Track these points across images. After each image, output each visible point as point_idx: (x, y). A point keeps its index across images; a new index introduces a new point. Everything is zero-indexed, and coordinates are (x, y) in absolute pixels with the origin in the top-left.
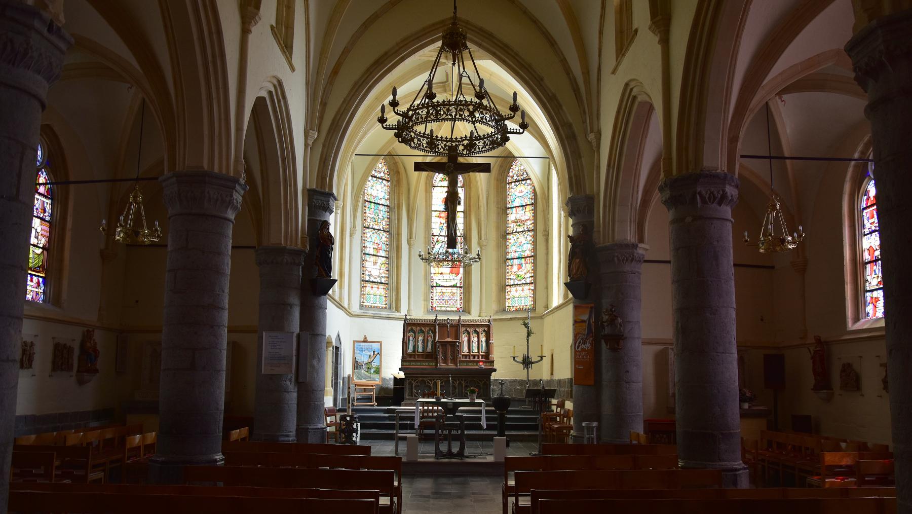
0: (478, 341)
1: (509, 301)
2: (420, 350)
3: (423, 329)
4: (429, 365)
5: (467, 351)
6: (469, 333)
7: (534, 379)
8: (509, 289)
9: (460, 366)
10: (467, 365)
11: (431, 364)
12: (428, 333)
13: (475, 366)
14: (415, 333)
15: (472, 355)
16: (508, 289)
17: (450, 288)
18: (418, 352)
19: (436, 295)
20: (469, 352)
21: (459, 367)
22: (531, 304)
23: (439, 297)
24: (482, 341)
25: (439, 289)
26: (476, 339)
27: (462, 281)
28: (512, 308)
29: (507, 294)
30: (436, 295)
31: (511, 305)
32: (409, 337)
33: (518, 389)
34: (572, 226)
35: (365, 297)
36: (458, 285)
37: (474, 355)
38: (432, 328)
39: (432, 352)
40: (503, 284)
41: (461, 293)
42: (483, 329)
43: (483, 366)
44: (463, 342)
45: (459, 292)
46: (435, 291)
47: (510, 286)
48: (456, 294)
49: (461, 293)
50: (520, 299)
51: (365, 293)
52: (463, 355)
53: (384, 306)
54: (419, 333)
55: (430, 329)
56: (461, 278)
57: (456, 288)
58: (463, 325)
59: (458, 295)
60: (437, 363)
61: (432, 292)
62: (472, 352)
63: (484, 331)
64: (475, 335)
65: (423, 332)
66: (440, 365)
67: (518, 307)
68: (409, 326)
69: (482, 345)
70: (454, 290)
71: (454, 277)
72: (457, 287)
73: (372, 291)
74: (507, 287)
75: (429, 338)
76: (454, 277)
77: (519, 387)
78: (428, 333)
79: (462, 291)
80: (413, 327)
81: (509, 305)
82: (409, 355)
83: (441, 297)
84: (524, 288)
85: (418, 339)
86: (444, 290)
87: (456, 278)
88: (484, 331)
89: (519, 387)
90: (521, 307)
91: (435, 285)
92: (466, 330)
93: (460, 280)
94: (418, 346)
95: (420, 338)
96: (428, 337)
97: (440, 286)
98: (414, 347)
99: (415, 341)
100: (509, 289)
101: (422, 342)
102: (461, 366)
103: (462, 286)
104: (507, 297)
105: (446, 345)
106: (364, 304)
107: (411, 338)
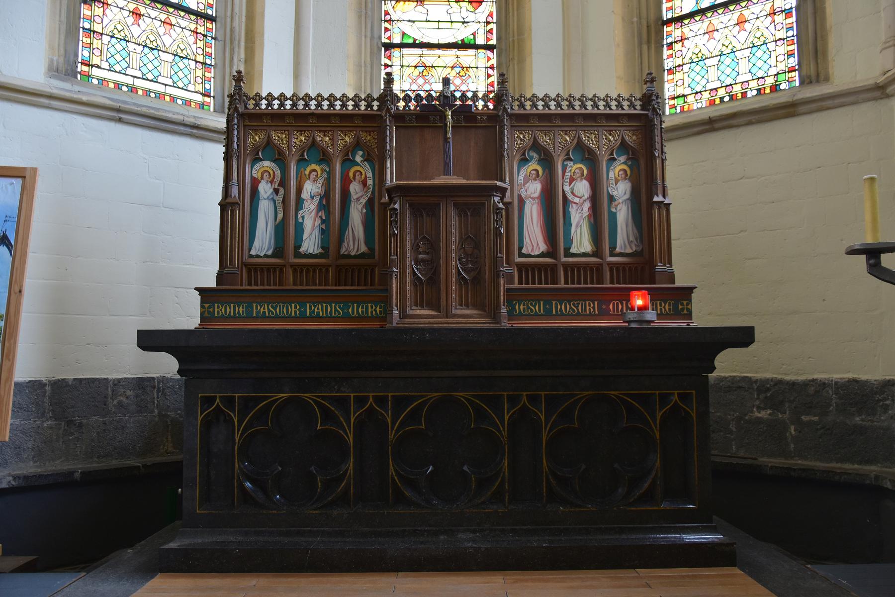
0: (595, 199)
1: (678, 76)
2: (310, 243)
3: (323, 139)
4: (347, 318)
5: (543, 247)
6: (547, 160)
7: (850, 376)
8: (677, 33)
9: (511, 315)
10: (548, 314)
11: (355, 310)
12: (348, 161)
13: (591, 316)
14: (280, 159)
15: (566, 266)
16: (673, 32)
17: (453, 51)
18: (298, 255)
19: (402, 77)
20: (552, 252)
21: (506, 324)
22: (782, 67)
23: (414, 81)
24: (611, 198)
25: (411, 56)
26: (583, 188)
27: (493, 26)
28: (691, 99)
29: (666, 53)
30: (402, 77)
31: (688, 91)
32: (255, 183)
33: (759, 421)
34: (606, 161)
35: (97, 43)
36: (481, 41)
37: (578, 266)
38: (366, 137)
39: (370, 254)
40: (652, 17)
41: (492, 68)
42: (613, 139)
43: (651, 315)
44: (522, 202)
45: (482, 63)
46: (396, 61)
47: (680, 19)
48: (472, 72)
49: (492, 68)
50: (728, 61)
51: (97, 28)
52: (521, 267)
53: (198, 98)
54: (301, 161)
55: (358, 145)
56: (491, 15)
57: (472, 52)
58: (522, 120)
59: (482, 73)
60: (386, 301)
61: (386, 66)
62: (568, 253)
63: (624, 147)
64: (576, 167)
65: (325, 158)
66: (404, 315)
67: (722, 92)
68: (256, 130)
69: (613, 217)
70: (467, 57)
71: (464, 14)
72: (476, 47)
73: (136, 31)
74: (666, 29)
75: (355, 188)
76: (464, 14)
77: (764, 414)
78: (348, 161)
79: (494, 62)
80: (274, 136)
81: (679, 91)
82: (255, 269)
83: (421, 81)
84: (746, 13)
85: (299, 190)
86: (430, 57)
87: (471, 17)
88: (624, 147)
89: (764, 414)
90: (737, 89)
91: (397, 40)
92: (536, 146)
93: (488, 23)
94: (299, 228)
95: (311, 188)
96: (346, 182)
97: (415, 45)
98: (281, 230)
99: (285, 201)
100: (677, 33)
101: (320, 207)
102: (521, 316)
103: (493, 42)
104: (668, 64)
105: (432, 211)
106: (95, 72)
107: (265, 189)
